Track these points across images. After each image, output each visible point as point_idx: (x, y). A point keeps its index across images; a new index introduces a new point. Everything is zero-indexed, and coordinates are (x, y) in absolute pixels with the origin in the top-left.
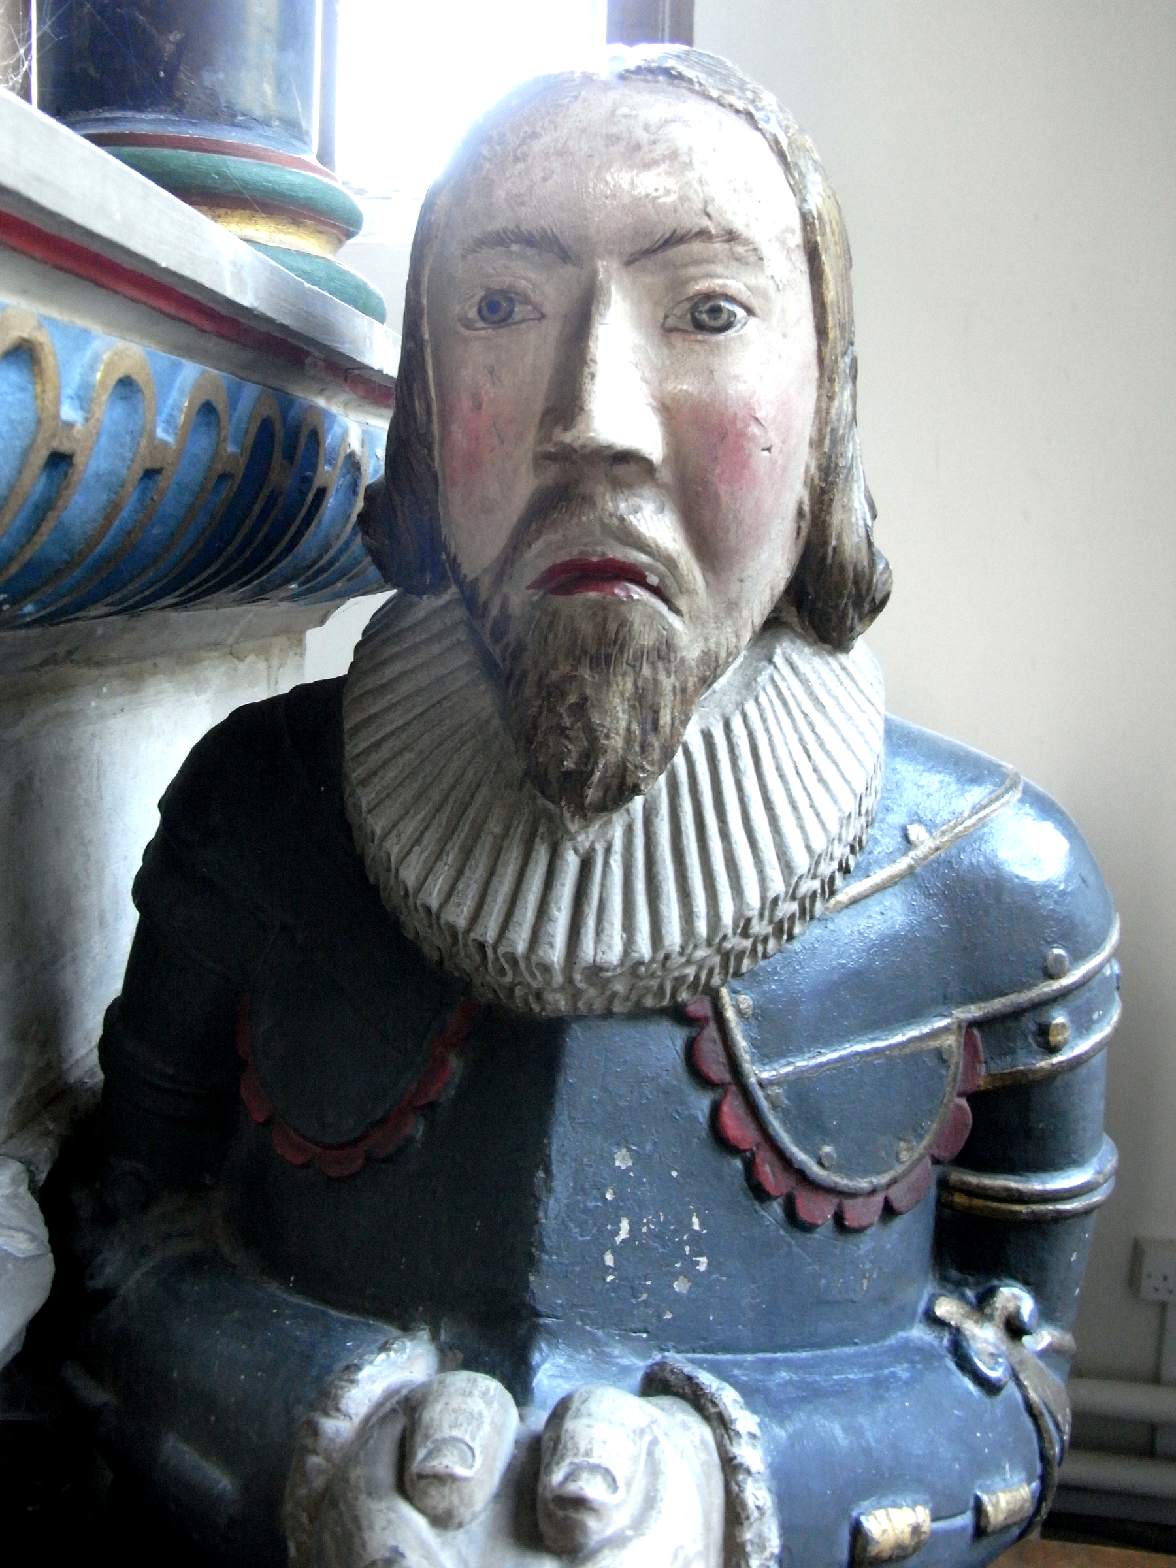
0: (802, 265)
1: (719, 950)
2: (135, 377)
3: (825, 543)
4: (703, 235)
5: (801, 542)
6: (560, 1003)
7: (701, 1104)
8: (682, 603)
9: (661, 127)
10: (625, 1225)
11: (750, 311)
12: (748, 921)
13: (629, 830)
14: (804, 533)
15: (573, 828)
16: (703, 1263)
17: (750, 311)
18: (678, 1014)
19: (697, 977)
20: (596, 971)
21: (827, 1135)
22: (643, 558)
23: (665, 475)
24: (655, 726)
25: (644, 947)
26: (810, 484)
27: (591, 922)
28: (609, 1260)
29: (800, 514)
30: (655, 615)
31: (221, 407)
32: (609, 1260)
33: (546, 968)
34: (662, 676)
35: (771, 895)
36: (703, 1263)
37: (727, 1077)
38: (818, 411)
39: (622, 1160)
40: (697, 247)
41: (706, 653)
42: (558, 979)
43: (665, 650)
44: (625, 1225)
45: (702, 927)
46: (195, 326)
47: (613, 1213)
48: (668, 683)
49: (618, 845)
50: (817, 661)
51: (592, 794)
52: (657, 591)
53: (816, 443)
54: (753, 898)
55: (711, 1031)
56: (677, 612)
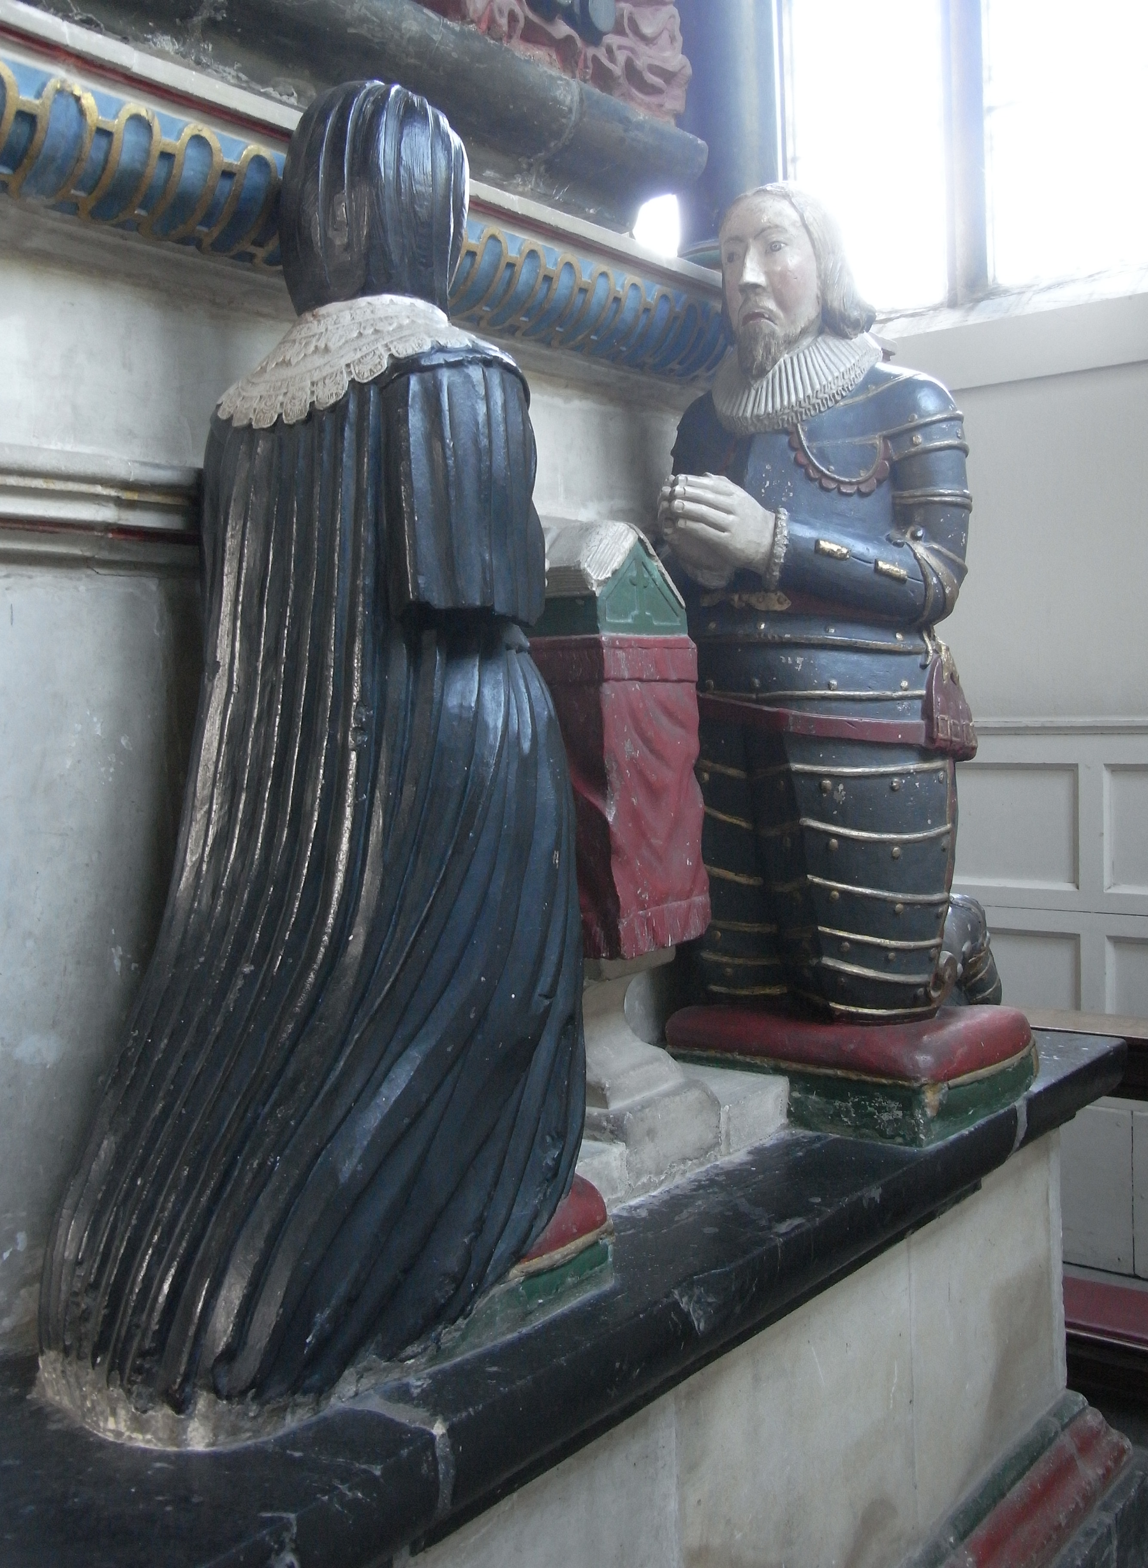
0: (803, 230)
1: (793, 411)
2: (38, 120)
3: (827, 304)
4: (769, 227)
5: (821, 305)
6: (752, 429)
7: (792, 455)
8: (777, 322)
9: (614, 316)
10: (768, 483)
11: (786, 244)
12: (800, 402)
13: (768, 383)
14: (820, 303)
15: (752, 382)
16: (791, 494)
17: (786, 244)
18: (786, 432)
19: (788, 419)
20: (758, 416)
21: (830, 463)
22: (763, 310)
23: (769, 289)
24: (770, 353)
25: (770, 409)
26: (819, 288)
27: (757, 405)
28: (763, 491)
29: (818, 297)
30: (768, 325)
31: (664, 109)
32: (763, 491)
33: (746, 418)
34: (771, 340)
35: (807, 395)
36: (791, 494)
37: (799, 447)
38: (817, 268)
39: (768, 467)
40: (769, 231)
41: (785, 335)
42: (750, 421)
43: (773, 334)
44: (768, 483)
45: (786, 403)
46: (968, 1085)
47: (765, 480)
48: (773, 342)
49: (765, 386)
50: (837, 343)
51: (754, 372)
52: (769, 319)
53: (819, 277)
54: (801, 396)
55: (795, 435)
56: (776, 324)
